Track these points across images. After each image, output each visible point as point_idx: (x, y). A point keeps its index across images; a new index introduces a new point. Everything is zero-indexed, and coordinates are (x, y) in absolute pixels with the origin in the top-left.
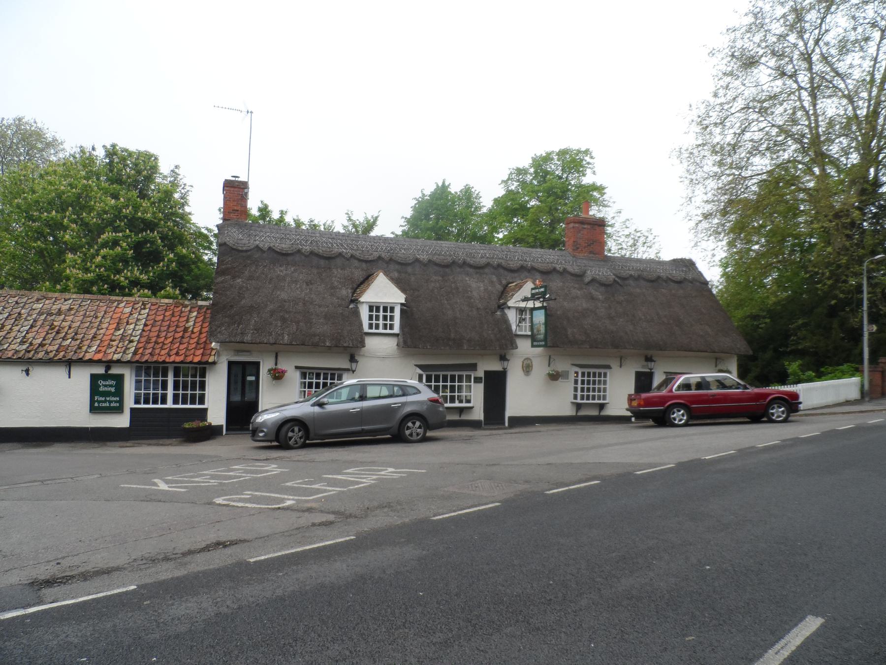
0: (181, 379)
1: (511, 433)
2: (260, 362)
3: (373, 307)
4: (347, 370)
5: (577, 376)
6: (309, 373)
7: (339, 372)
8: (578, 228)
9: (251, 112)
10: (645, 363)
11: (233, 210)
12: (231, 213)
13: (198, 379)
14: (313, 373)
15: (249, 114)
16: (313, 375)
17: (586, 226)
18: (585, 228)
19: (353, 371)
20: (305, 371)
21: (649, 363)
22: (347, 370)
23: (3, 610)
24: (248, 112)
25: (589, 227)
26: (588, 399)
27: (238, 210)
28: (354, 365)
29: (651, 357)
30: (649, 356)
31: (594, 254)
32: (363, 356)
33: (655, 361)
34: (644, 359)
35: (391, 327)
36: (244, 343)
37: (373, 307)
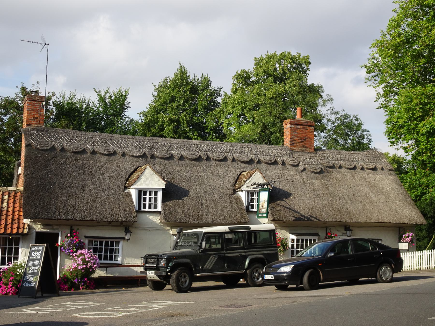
0: (109, 247)
1: (141, 292)
2: (59, 233)
3: (141, 191)
4: (123, 239)
5: (294, 242)
6: (95, 241)
7: (117, 240)
8: (294, 128)
9: (49, 45)
10: (345, 232)
11: (33, 118)
12: (32, 120)
13: (98, 247)
14: (97, 241)
15: (46, 46)
16: (97, 243)
17: (299, 127)
18: (299, 128)
19: (128, 240)
20: (91, 239)
21: (348, 232)
22: (123, 239)
23: (434, 320)
24: (45, 44)
25: (302, 127)
26: (106, 258)
27: (37, 118)
28: (128, 235)
29: (349, 227)
30: (347, 227)
31: (306, 148)
32: (135, 227)
33: (352, 230)
34: (343, 229)
35: (155, 207)
36: (60, 220)
37: (141, 191)
